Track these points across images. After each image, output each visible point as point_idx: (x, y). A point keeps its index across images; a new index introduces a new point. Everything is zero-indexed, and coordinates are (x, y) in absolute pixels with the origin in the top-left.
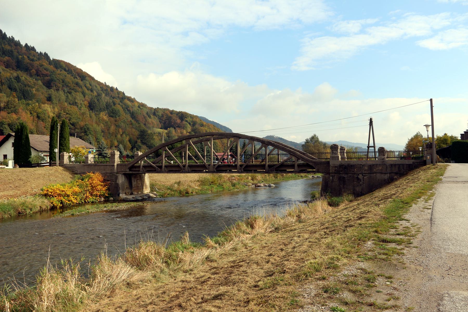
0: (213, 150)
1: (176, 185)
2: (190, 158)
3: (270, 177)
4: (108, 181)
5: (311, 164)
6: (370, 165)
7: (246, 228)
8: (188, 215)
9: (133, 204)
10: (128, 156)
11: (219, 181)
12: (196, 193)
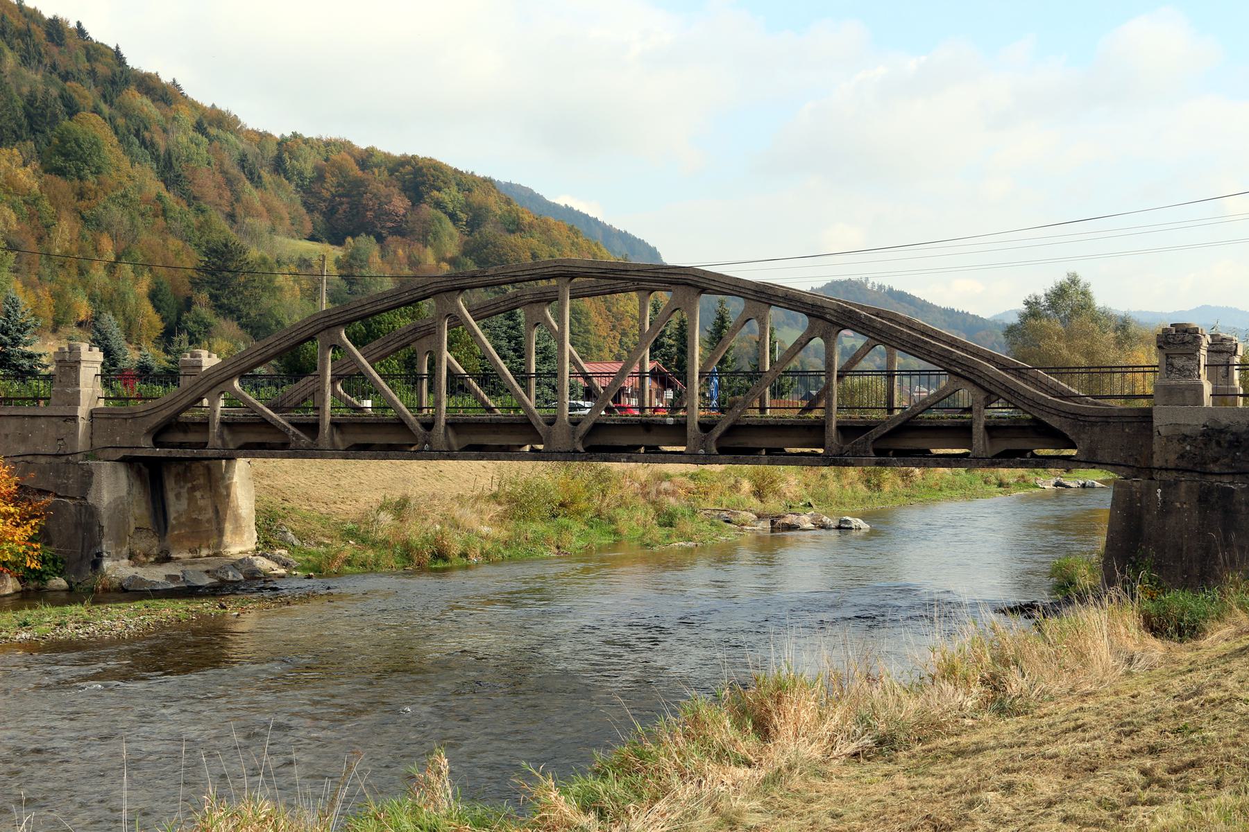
0: (568, 346)
1: (386, 518)
2: (457, 385)
3: (847, 484)
4: (46, 493)
5: (1054, 422)
7: (733, 733)
8: (444, 666)
9: (169, 610)
10: (144, 372)
11: (596, 501)
12: (486, 555)
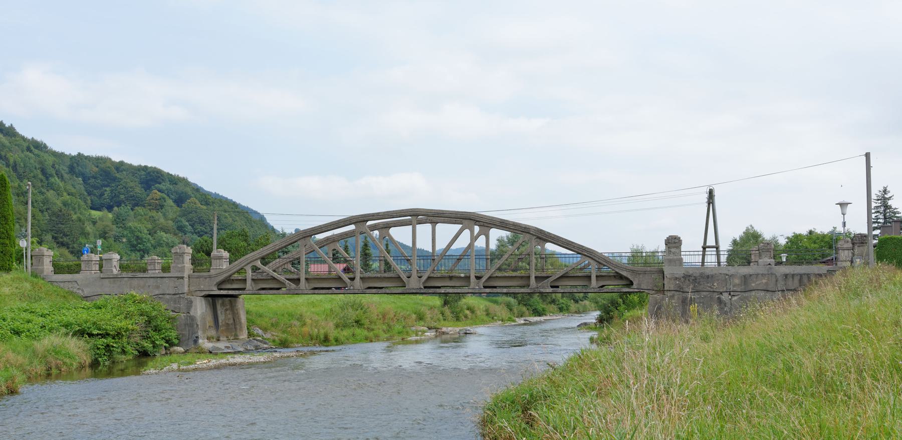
6: (745, 276)
